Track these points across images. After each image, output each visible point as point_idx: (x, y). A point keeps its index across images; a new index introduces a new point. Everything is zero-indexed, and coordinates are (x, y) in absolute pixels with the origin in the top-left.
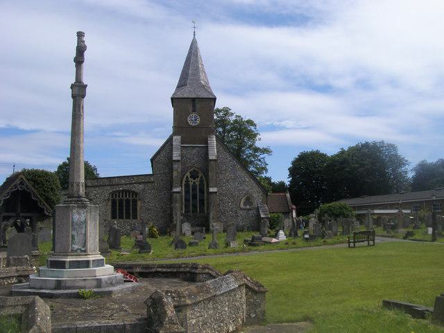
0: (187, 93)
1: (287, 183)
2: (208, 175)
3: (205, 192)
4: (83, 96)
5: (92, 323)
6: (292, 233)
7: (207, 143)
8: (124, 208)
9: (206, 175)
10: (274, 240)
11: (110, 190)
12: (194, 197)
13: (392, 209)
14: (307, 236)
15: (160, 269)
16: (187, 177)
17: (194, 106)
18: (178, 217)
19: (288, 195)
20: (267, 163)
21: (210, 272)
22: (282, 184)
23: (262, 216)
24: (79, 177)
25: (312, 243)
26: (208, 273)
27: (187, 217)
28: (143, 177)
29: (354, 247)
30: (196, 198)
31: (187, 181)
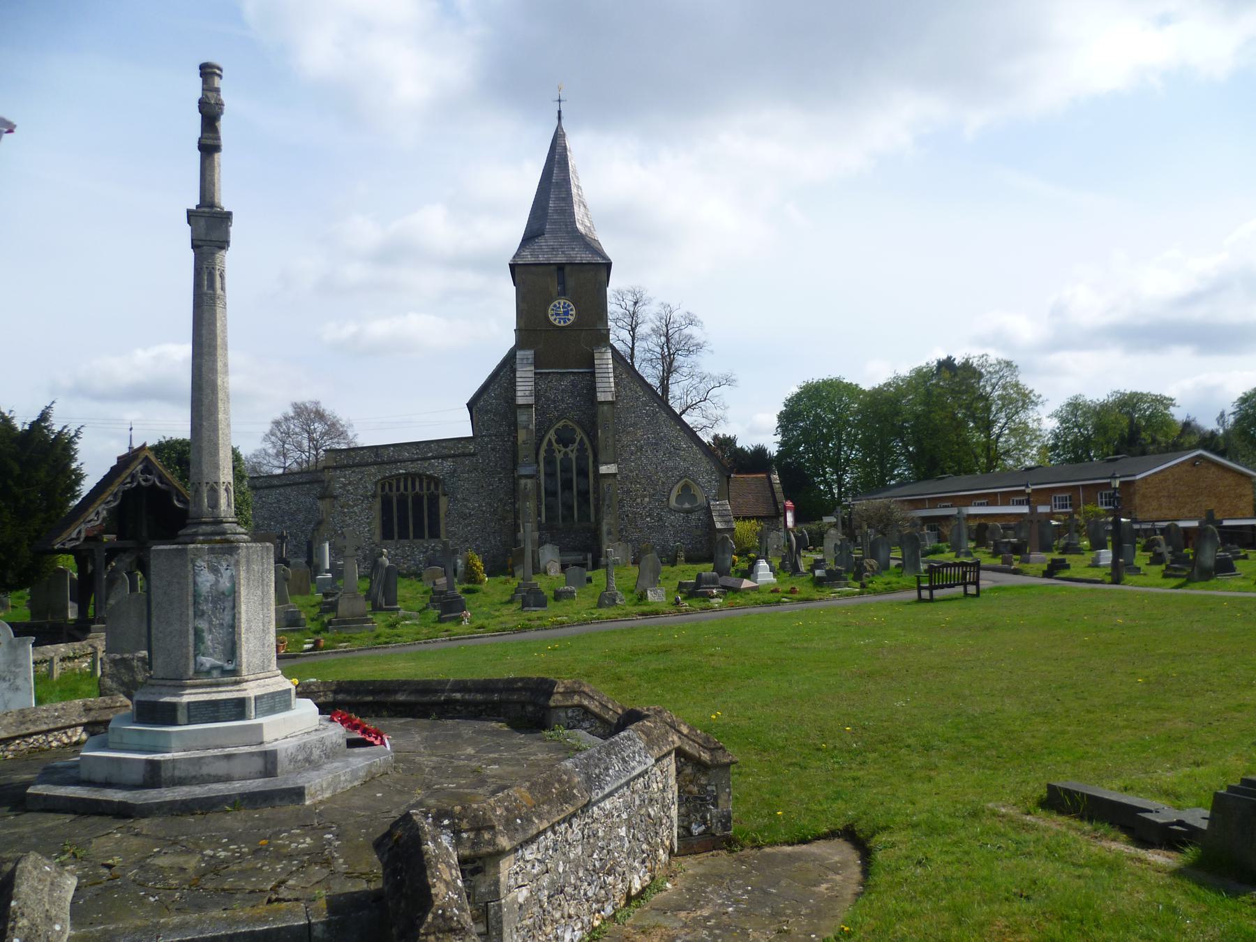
0: (549, 252)
1: (773, 449)
3: (591, 476)
4: (223, 244)
6: (788, 566)
7: (592, 365)
8: (410, 513)
9: (593, 438)
10: (746, 583)
11: (374, 475)
12: (567, 485)
13: (1007, 504)
14: (818, 573)
15: (458, 696)
17: (562, 282)
18: (528, 532)
19: (775, 477)
21: (586, 703)
22: (760, 452)
23: (719, 526)
24: (216, 467)
25: (827, 592)
26: (580, 706)
27: (549, 532)
28: (450, 444)
29: (931, 600)
30: (571, 488)
31: (550, 451)
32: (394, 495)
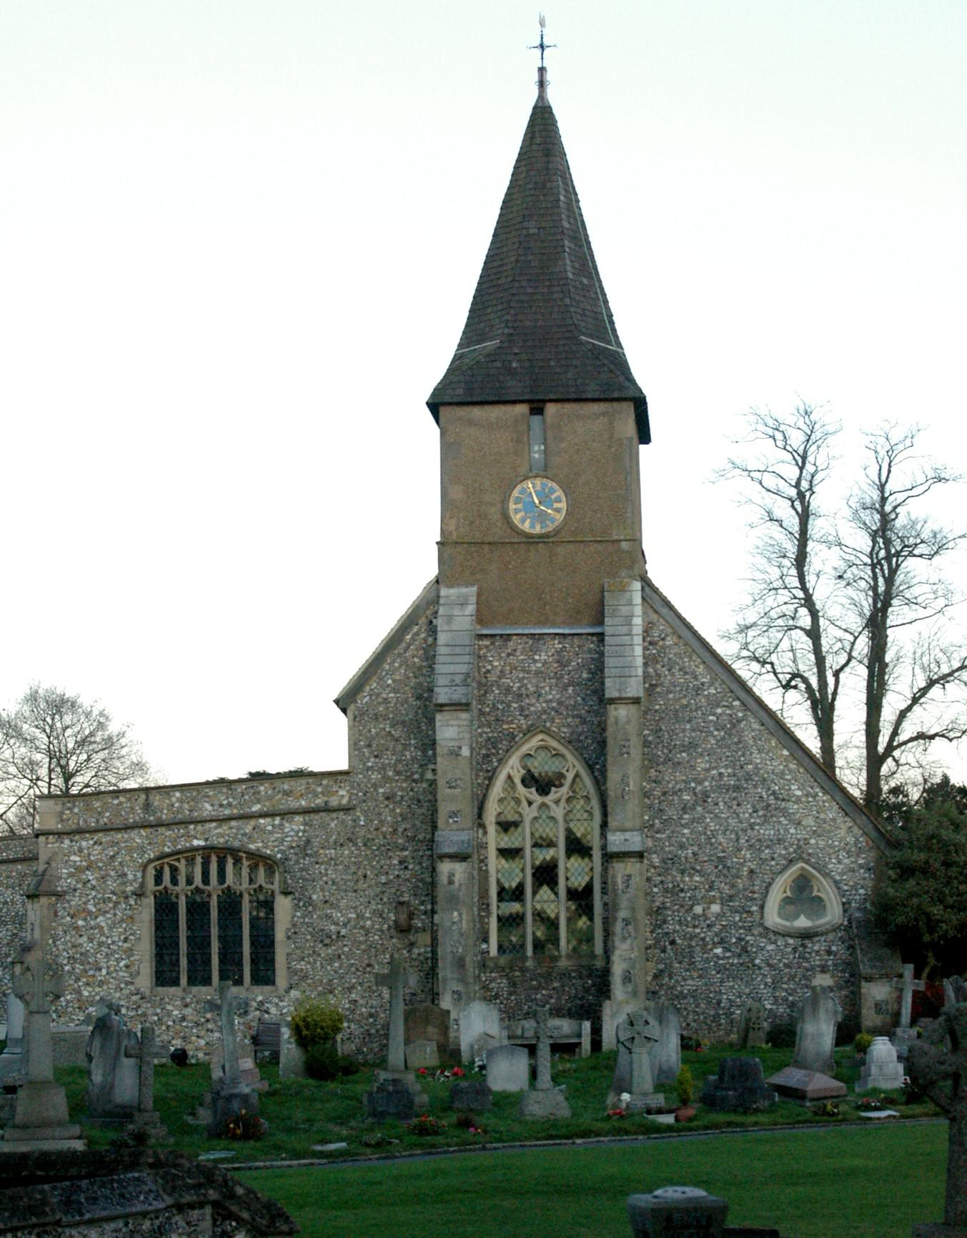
2: (603, 771)
5: (181, 1196)
11: (144, 846)
32: (181, 893)
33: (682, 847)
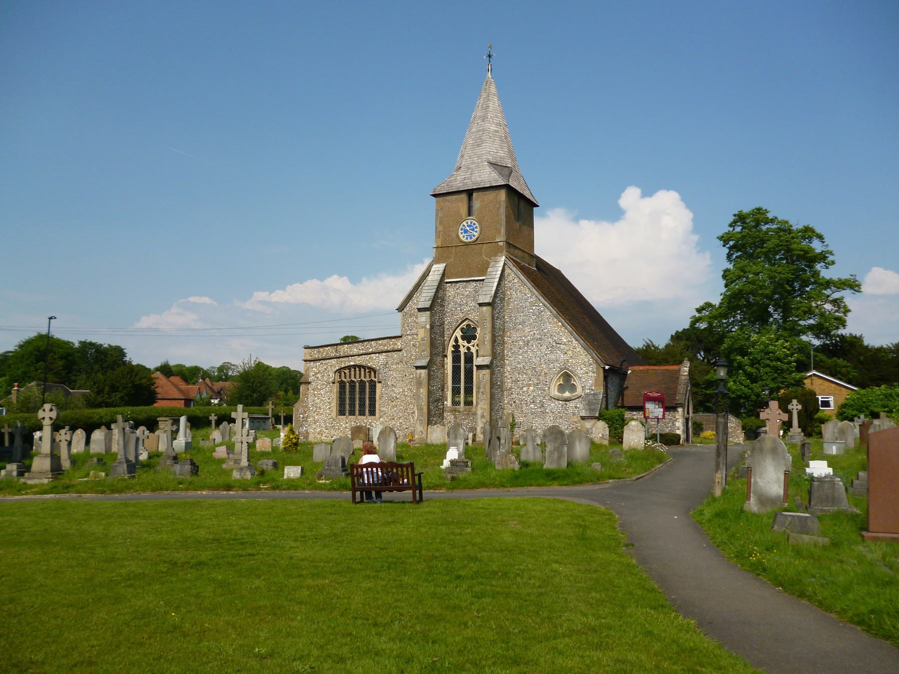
16: (456, 340)
20: (850, 307)
31: (456, 347)
33: (519, 363)
